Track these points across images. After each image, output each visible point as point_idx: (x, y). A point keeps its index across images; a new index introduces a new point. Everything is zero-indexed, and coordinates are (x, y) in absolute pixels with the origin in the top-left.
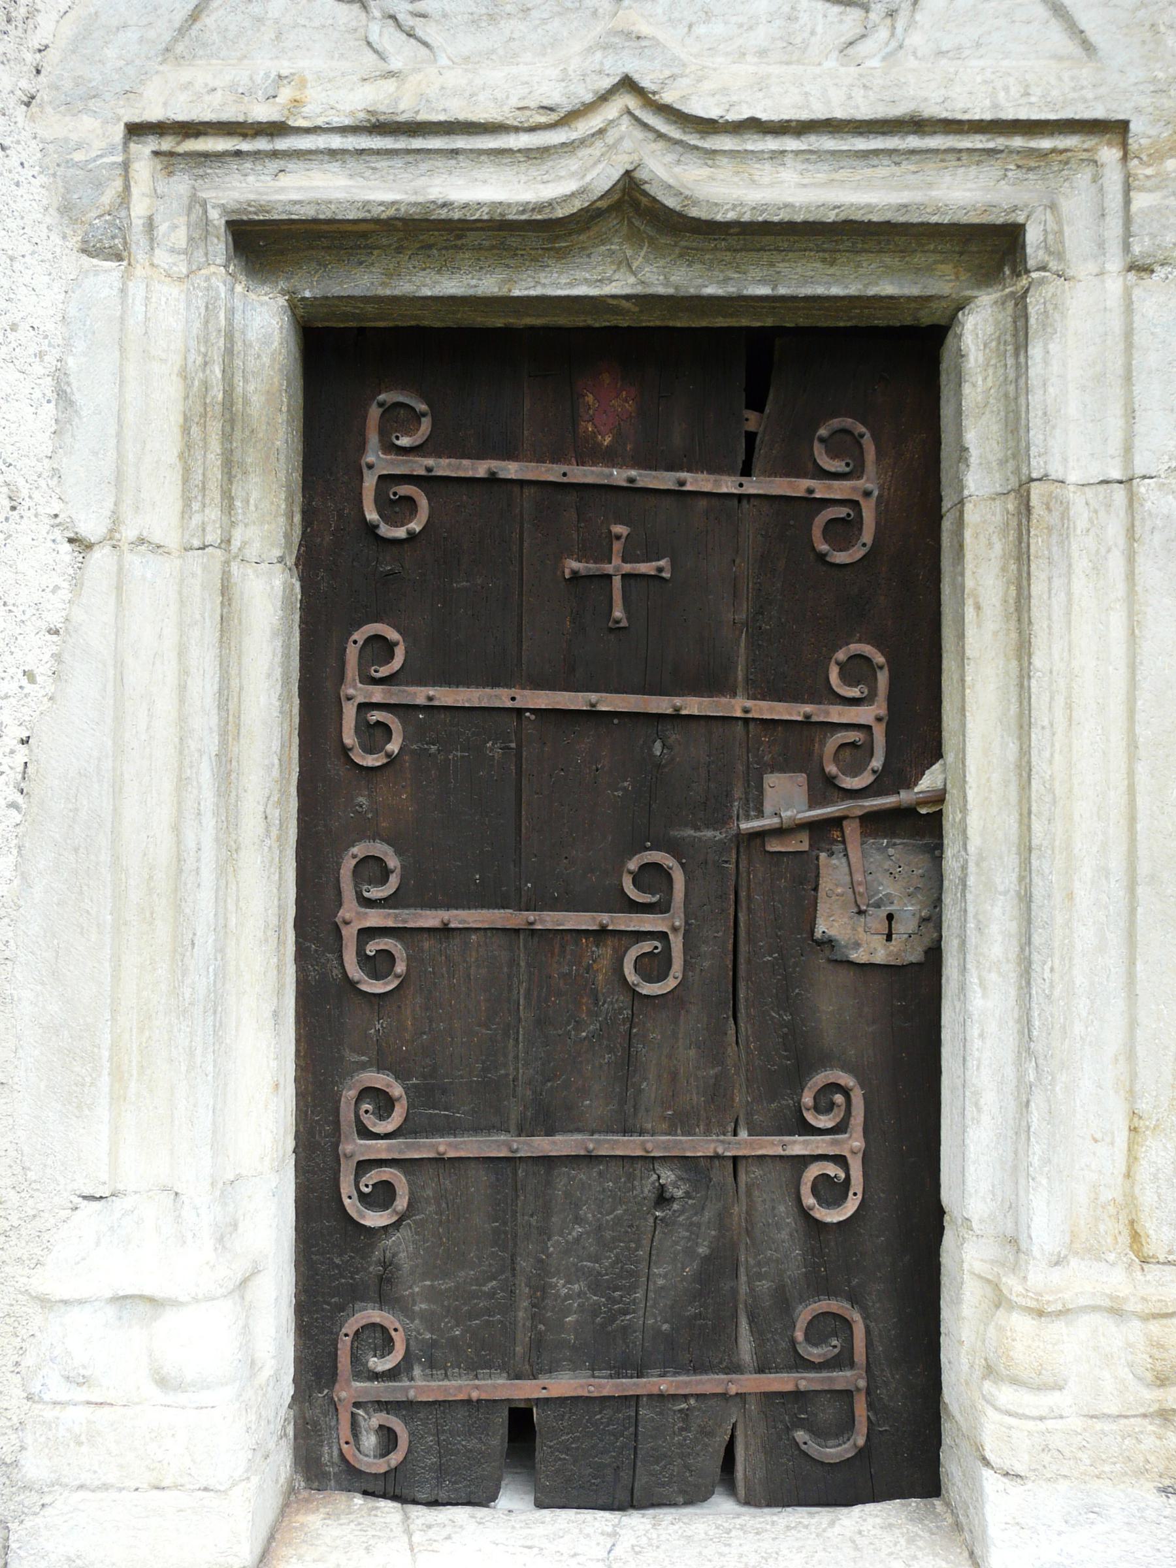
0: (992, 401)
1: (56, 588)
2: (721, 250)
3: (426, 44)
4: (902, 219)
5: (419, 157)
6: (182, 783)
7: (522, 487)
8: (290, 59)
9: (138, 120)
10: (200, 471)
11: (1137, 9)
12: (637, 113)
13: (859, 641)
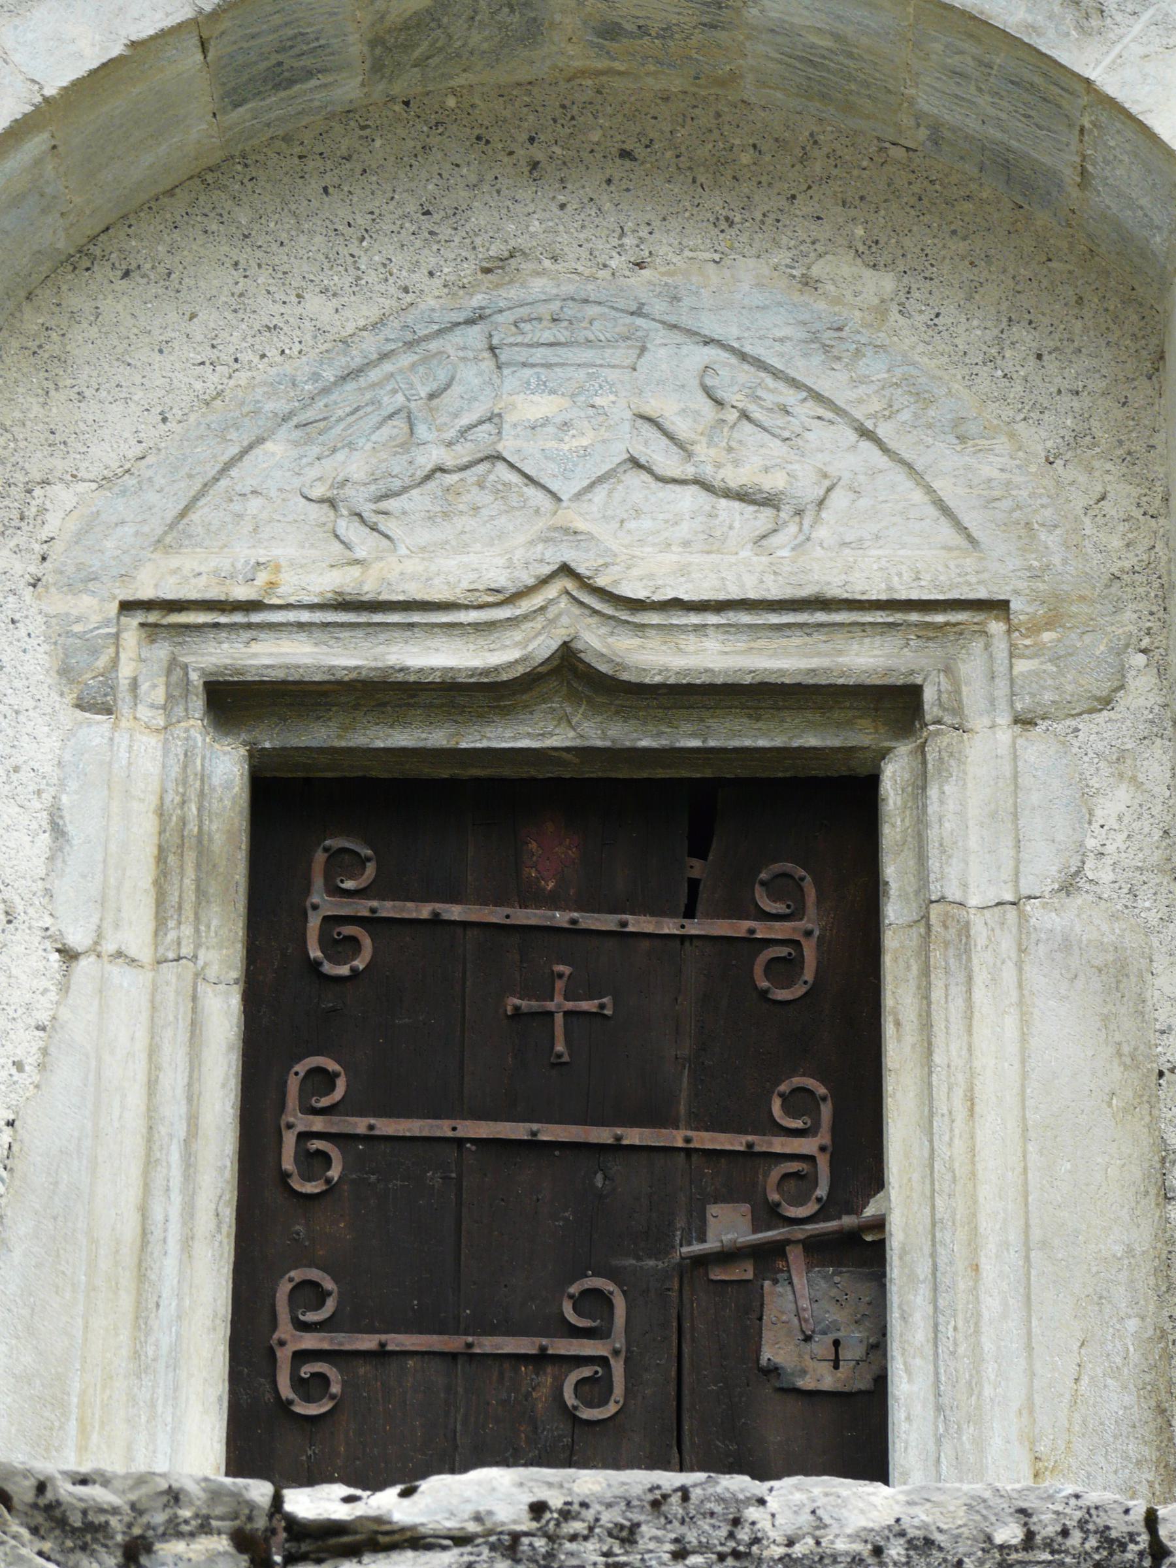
0: (909, 839)
1: (46, 990)
2: (653, 708)
3: (387, 537)
4: (811, 682)
5: (378, 629)
6: (149, 1163)
7: (465, 930)
8: (266, 548)
9: (131, 599)
10: (177, 894)
11: (1013, 510)
12: (574, 593)
13: (804, 1075)
